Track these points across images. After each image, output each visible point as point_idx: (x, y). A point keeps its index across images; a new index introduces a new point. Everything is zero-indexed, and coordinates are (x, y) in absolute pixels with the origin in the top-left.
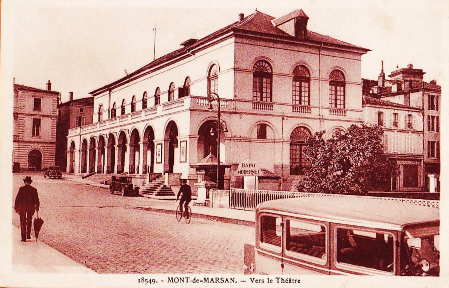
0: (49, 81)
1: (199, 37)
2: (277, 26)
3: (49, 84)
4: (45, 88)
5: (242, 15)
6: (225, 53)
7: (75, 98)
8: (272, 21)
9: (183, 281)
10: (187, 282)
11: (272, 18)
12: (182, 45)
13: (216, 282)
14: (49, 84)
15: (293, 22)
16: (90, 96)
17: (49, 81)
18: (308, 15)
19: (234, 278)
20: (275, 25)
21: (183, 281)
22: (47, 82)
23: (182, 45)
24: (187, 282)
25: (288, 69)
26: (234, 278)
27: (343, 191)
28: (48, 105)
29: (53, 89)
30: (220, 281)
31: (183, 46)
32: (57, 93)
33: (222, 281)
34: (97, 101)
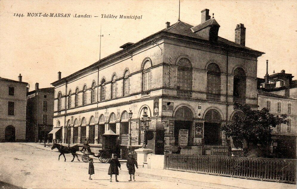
0: (20, 74)
1: (135, 41)
2: (195, 32)
3: (20, 77)
4: (17, 79)
5: (168, 23)
6: (155, 52)
7: (40, 87)
8: (191, 29)
9: (37, 16)
10: (40, 16)
11: (191, 26)
12: (121, 47)
13: (58, 17)
14: (20, 77)
15: (209, 28)
16: (52, 86)
17: (20, 74)
18: (219, 23)
19: (70, 14)
20: (193, 31)
21: (37, 16)
22: (19, 75)
23: (121, 47)
24: (40, 16)
25: (203, 64)
26: (70, 14)
27: (182, 36)
28: (19, 92)
29: (23, 80)
30: (61, 16)
31: (123, 49)
32: (27, 84)
33: (62, 16)
34: (57, 90)
